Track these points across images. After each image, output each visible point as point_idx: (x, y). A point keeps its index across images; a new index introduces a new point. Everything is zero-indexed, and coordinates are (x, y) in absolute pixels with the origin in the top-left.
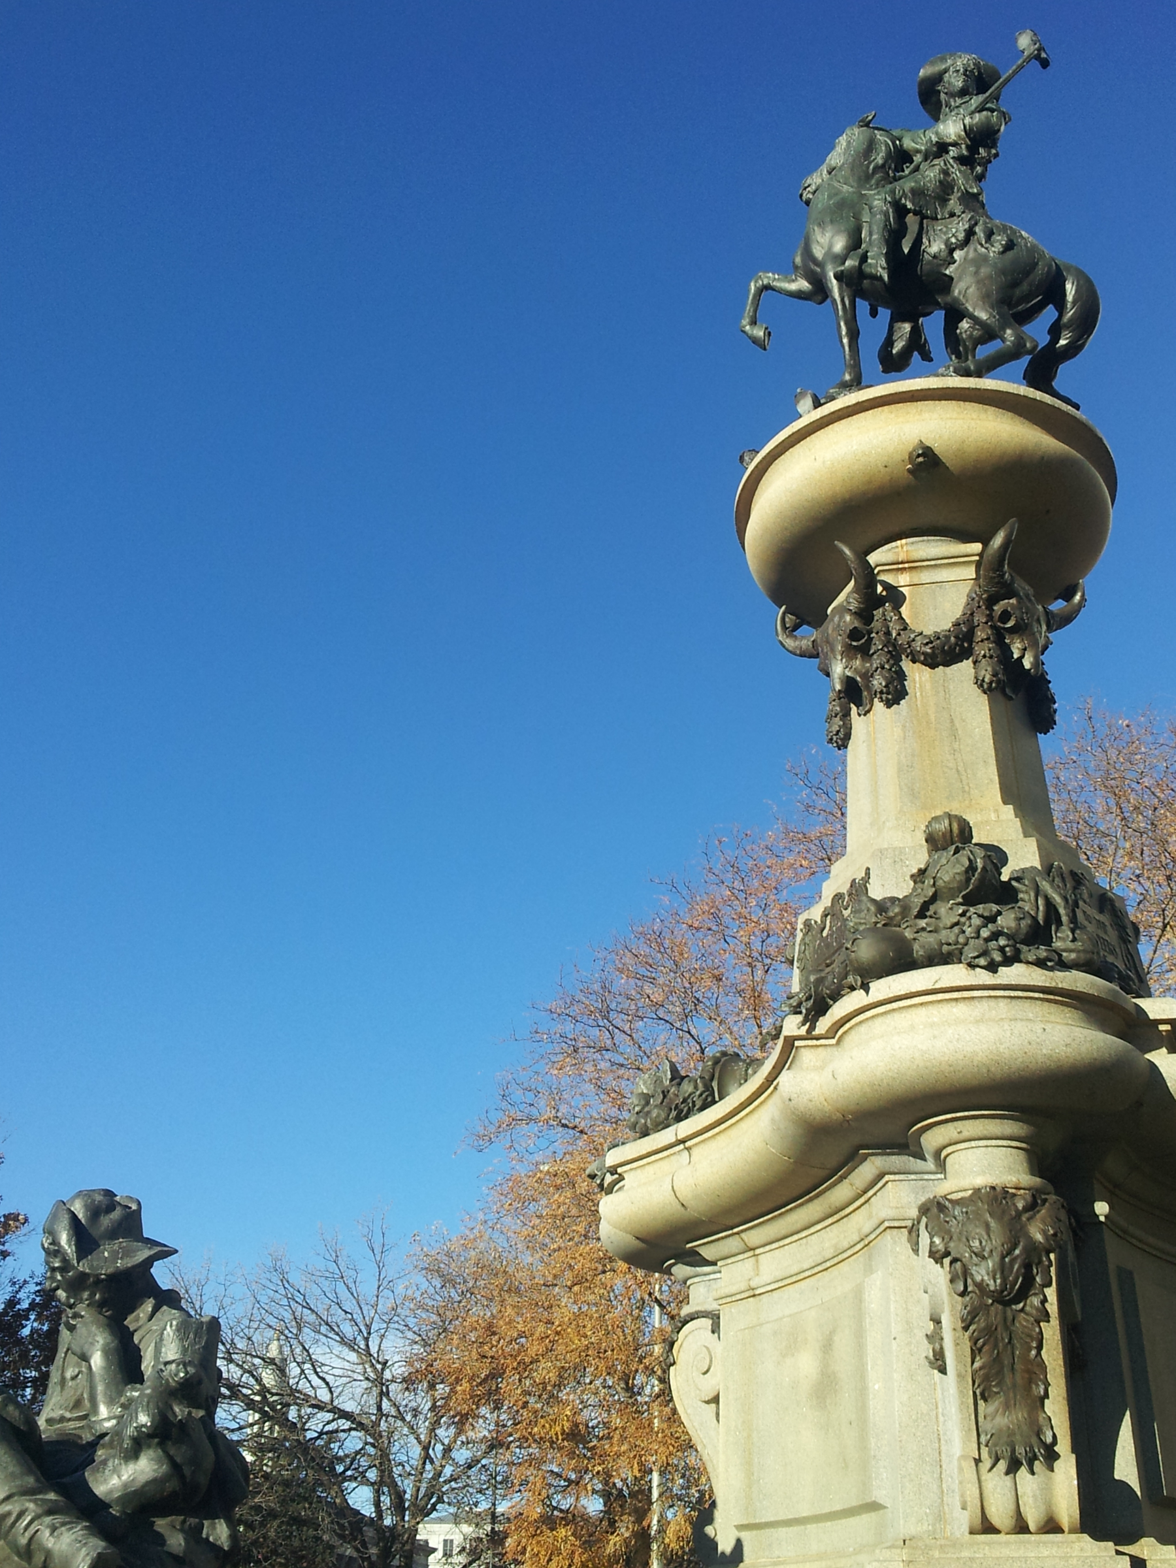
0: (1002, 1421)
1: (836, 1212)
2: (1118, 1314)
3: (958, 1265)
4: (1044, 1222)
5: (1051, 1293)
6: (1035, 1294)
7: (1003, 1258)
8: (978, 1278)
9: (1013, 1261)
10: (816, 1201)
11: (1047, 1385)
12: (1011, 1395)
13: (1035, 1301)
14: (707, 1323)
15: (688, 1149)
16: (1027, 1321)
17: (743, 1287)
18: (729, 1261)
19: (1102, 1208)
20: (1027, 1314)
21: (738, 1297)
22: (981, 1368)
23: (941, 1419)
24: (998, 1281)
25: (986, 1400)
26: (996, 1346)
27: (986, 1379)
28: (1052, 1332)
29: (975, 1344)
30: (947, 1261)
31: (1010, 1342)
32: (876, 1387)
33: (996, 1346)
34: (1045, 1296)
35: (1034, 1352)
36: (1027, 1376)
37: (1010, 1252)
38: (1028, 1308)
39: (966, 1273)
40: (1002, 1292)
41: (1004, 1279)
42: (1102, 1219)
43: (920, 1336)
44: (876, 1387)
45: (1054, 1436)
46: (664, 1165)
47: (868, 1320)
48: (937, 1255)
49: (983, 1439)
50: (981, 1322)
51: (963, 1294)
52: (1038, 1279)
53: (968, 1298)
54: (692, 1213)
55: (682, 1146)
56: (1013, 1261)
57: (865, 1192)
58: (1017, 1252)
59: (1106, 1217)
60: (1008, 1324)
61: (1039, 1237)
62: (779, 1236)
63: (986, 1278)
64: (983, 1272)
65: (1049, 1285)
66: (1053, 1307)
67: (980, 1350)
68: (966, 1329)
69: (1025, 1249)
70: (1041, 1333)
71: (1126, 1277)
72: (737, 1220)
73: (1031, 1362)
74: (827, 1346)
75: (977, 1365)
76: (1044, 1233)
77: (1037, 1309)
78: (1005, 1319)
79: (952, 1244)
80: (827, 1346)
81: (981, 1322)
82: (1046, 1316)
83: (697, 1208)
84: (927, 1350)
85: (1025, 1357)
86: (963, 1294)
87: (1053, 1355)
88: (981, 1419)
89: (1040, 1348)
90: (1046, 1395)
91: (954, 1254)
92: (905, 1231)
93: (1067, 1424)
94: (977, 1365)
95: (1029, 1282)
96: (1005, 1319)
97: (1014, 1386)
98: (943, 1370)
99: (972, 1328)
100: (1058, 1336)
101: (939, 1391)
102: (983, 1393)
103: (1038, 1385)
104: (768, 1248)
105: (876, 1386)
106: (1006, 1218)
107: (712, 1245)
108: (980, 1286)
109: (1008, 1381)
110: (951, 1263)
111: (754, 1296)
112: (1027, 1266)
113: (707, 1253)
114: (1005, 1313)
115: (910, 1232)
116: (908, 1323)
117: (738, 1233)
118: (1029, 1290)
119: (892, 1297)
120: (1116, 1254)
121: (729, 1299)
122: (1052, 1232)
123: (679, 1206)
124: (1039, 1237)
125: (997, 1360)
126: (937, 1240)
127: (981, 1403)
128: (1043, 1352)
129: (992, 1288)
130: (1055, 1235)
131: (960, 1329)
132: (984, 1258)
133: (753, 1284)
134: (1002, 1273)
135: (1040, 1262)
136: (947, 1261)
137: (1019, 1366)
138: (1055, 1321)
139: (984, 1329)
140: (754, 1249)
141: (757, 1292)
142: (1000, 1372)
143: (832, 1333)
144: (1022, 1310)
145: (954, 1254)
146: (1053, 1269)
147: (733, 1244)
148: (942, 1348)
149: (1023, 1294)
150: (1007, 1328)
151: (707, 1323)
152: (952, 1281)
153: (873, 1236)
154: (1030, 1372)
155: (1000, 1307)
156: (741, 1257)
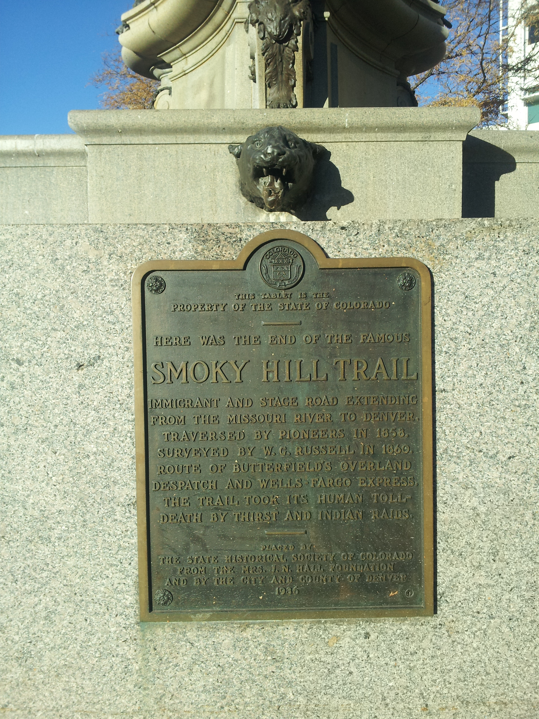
0: (276, 95)
1: (218, 28)
2: (329, 61)
3: (262, 26)
4: (300, 7)
5: (300, 38)
6: (293, 39)
7: (281, 21)
8: (269, 30)
9: (285, 22)
10: (209, 23)
11: (295, 80)
12: (281, 85)
13: (293, 42)
14: (167, 91)
15: (156, 7)
16: (289, 51)
17: (180, 71)
18: (175, 62)
19: (327, 14)
20: (289, 48)
21: (179, 76)
22: (269, 73)
23: (253, 101)
24: (278, 31)
25: (270, 87)
26: (275, 63)
27: (271, 77)
28: (299, 56)
29: (267, 61)
30: (257, 24)
31: (281, 61)
32: (229, 92)
33: (275, 63)
34: (297, 40)
35: (291, 65)
36: (287, 76)
37: (283, 19)
38: (290, 45)
39: (265, 29)
40: (279, 35)
41: (280, 30)
42: (327, 19)
43: (247, 68)
44: (229, 92)
45: (297, 102)
46: (146, 17)
47: (226, 65)
48: (253, 22)
49: (268, 103)
50: (270, 52)
51: (263, 39)
52: (295, 32)
53: (265, 40)
54: (158, 36)
55: (153, 7)
56: (285, 22)
57: (229, 13)
58: (287, 18)
59: (328, 18)
60: (281, 52)
61: (297, 13)
62: (195, 46)
63: (273, 30)
64: (272, 27)
65: (299, 35)
66: (300, 45)
67: (269, 64)
68: (263, 54)
69: (290, 18)
70: (294, 56)
71: (334, 47)
72: (177, 40)
73: (289, 70)
74: (211, 85)
75: (267, 71)
76: (299, 12)
77: (294, 45)
78: (280, 50)
79: (260, 17)
80: (211, 85)
81: (270, 52)
82: (297, 49)
83: (160, 33)
84: (249, 73)
85: (287, 68)
86: (263, 39)
87: (299, 68)
88: (268, 96)
89: (293, 63)
90: (294, 86)
91: (260, 21)
92: (243, 24)
93: (302, 98)
94: (267, 71)
95: (291, 33)
96: (280, 50)
97: (282, 81)
98: (255, 82)
99: (266, 54)
100: (301, 58)
101: (253, 90)
102: (269, 85)
103: (291, 80)
104: (191, 53)
105: (228, 91)
106: (284, 4)
107: (168, 55)
108: (270, 33)
109: (280, 78)
110: (259, 25)
111: (185, 74)
112: (291, 25)
113: (167, 59)
114: (280, 47)
115: (245, 23)
116: (242, 63)
117: (178, 47)
118: (291, 37)
119: (236, 52)
120: (330, 38)
121: (175, 78)
122: (302, 11)
123: (152, 33)
124: (297, 13)
125: (275, 69)
126: (254, 15)
127: (268, 88)
128: (295, 66)
129: (275, 34)
130: (304, 13)
131: (261, 55)
132: (272, 21)
133: (185, 69)
134: (280, 27)
135: (296, 24)
136: (257, 24)
137: (285, 72)
138: (300, 51)
139: (271, 54)
140: (185, 55)
141: (186, 72)
142: (276, 75)
143: (214, 78)
144: (287, 46)
145: (260, 21)
146: (301, 28)
147: (176, 53)
148: (254, 69)
149: (288, 38)
150: (280, 54)
151: (167, 91)
152: (259, 33)
153: (230, 31)
154: (289, 75)
155: (278, 44)
156: (180, 59)
